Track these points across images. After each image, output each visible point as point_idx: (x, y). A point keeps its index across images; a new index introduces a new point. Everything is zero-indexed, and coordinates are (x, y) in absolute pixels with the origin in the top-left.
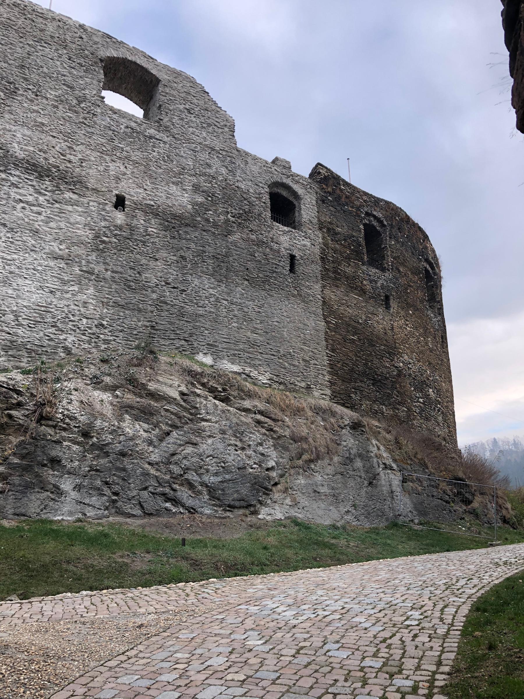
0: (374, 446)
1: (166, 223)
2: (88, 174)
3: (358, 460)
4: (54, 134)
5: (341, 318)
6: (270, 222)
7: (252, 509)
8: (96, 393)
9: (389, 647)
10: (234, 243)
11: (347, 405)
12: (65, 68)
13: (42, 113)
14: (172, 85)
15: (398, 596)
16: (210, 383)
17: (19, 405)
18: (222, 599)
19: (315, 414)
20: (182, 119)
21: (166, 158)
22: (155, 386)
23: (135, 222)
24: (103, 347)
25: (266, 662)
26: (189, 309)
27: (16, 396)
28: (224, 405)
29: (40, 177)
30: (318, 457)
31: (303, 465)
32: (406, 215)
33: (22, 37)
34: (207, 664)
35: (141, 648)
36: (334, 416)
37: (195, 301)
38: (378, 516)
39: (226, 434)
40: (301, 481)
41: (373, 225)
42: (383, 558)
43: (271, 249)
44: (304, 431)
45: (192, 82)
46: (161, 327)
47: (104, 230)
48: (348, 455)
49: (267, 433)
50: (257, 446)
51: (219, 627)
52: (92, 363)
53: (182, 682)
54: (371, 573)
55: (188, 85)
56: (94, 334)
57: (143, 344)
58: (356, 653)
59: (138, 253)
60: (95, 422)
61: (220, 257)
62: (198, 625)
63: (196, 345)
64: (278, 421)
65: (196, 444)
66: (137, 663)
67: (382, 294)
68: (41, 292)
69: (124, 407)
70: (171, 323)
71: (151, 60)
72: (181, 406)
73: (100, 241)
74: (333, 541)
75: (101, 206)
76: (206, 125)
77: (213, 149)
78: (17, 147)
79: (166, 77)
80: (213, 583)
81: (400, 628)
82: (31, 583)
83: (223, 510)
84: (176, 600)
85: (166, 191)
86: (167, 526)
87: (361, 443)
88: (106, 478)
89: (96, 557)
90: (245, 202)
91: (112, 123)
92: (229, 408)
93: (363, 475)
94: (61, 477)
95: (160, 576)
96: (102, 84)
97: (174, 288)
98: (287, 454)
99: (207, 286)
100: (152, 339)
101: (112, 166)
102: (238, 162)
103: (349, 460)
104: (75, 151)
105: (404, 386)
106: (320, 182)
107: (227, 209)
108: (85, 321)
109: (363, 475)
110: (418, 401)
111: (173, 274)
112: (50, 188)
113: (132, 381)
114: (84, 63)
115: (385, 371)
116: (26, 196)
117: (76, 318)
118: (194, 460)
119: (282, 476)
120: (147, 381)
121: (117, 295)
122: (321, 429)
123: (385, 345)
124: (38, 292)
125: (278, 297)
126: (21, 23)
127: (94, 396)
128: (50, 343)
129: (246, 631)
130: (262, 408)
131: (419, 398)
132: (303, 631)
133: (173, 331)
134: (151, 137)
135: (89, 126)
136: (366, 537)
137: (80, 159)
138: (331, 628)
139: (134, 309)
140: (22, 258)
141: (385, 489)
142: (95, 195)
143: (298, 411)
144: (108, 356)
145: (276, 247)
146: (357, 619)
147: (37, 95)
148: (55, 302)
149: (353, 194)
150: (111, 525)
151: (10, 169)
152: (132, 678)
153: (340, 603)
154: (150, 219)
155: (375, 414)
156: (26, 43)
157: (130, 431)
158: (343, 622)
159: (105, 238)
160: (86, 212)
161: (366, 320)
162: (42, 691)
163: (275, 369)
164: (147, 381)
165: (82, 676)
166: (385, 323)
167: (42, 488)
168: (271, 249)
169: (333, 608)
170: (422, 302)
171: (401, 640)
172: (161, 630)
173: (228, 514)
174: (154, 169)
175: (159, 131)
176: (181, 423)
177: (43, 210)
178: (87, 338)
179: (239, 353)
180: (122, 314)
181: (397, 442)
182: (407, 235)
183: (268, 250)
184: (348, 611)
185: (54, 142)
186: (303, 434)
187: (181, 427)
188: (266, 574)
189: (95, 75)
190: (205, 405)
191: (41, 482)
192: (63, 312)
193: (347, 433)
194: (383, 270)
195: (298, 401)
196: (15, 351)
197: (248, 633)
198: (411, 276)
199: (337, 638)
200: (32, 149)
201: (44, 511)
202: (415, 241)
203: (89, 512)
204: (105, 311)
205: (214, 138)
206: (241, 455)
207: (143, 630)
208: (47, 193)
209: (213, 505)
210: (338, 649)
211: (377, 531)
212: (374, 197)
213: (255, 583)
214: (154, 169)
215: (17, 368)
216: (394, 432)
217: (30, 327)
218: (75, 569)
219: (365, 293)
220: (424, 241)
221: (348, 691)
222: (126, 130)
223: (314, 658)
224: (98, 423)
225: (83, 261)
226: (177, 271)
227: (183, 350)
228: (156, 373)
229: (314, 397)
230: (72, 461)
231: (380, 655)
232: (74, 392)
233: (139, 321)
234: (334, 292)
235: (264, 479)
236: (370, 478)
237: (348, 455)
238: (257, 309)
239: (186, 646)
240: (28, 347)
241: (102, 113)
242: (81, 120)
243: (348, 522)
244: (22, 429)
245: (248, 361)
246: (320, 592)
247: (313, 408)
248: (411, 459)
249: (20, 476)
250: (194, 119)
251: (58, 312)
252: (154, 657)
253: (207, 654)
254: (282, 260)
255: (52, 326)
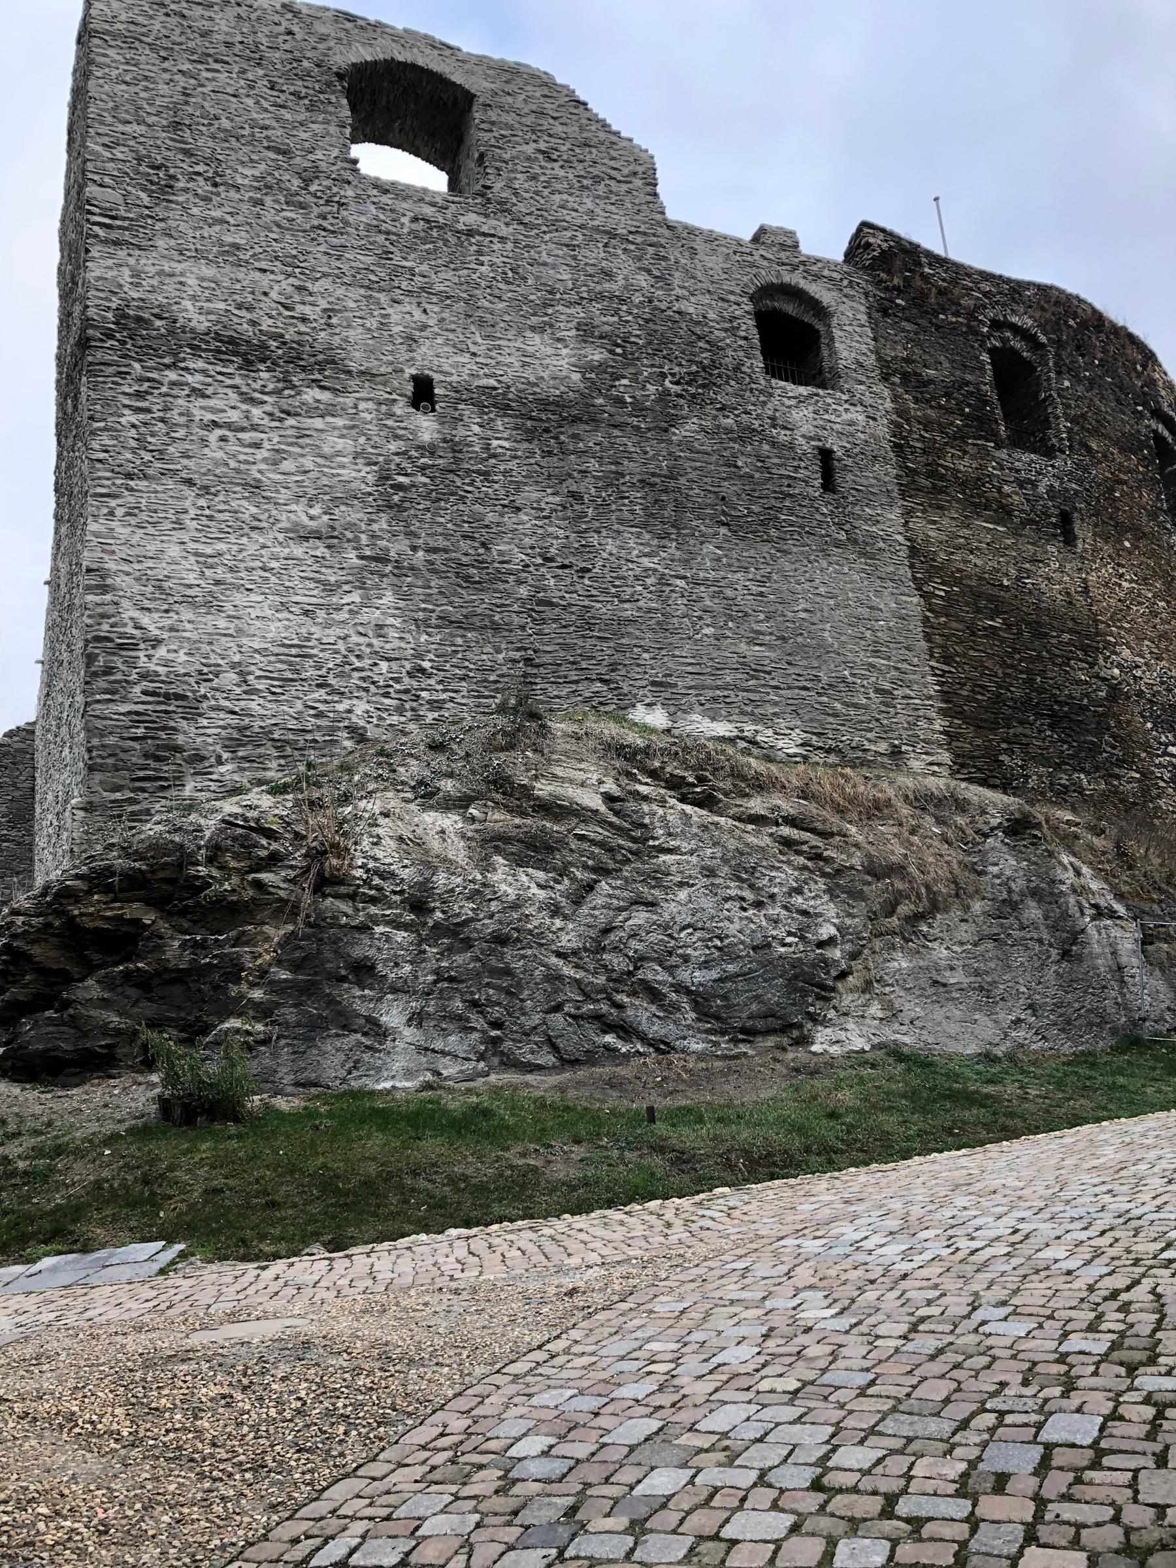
0: (1066, 869)
1: (529, 423)
2: (346, 340)
3: (1032, 903)
4: (263, 265)
5: (958, 582)
6: (763, 382)
7: (795, 1033)
8: (429, 817)
9: (1125, 1308)
10: (687, 445)
11: (991, 781)
12: (266, 110)
13: (232, 221)
14: (503, 100)
15: (1146, 1197)
16: (668, 769)
17: (274, 860)
18: (744, 1229)
19: (918, 812)
20: (534, 178)
21: (510, 274)
22: (549, 788)
23: (461, 432)
24: (430, 716)
25: (844, 1352)
26: (602, 609)
27: (264, 842)
28: (704, 812)
29: (248, 365)
30: (935, 907)
31: (901, 926)
32: (1094, 311)
33: (165, 59)
34: (715, 1361)
35: (575, 1334)
36: (964, 811)
37: (613, 590)
38: (1091, 1024)
39: (716, 876)
40: (901, 962)
41: (1012, 348)
42: (1110, 1118)
43: (773, 444)
44: (896, 851)
45: (546, 84)
46: (546, 659)
47: (397, 459)
48: (1005, 895)
49: (810, 864)
50: (790, 895)
51: (739, 1286)
52: (411, 755)
53: (666, 1399)
54: (1080, 1152)
55: (538, 94)
56: (406, 691)
57: (513, 701)
58: (1048, 1324)
59: (476, 501)
60: (434, 879)
61: (657, 480)
62: (694, 1285)
63: (626, 690)
64: (832, 835)
65: (653, 904)
66: (569, 1365)
67: (1052, 510)
68: (286, 615)
69: (490, 841)
70: (565, 647)
71: (448, 52)
72: (611, 824)
73: (392, 486)
74: (989, 1089)
75: (384, 408)
76: (590, 182)
77: (612, 235)
78: (190, 308)
79: (486, 85)
80: (724, 1196)
81: (1151, 1267)
82: (346, 1219)
83: (730, 1040)
84: (645, 1237)
85: (518, 349)
86: (613, 1083)
87: (1035, 863)
88: (472, 993)
89: (470, 1159)
90: (701, 344)
91: (382, 217)
92: (716, 819)
93: (1046, 936)
94: (380, 999)
95: (608, 1190)
96: (348, 131)
97: (564, 567)
98: (860, 908)
99: (635, 552)
100: (530, 687)
101: (395, 314)
102: (674, 254)
103: (1009, 906)
104: (311, 294)
105: (1129, 722)
106: (872, 267)
107: (661, 367)
108: (384, 666)
109: (1046, 936)
110: (1165, 754)
111: (558, 534)
112: (271, 387)
113: (500, 783)
114: (304, 91)
115: (1077, 692)
116: (224, 411)
117: (366, 663)
118: (654, 937)
119: (854, 956)
120: (531, 779)
121: (445, 601)
122: (935, 843)
123: (1070, 631)
124: (279, 615)
125: (803, 553)
126: (158, 26)
127: (425, 822)
128: (319, 722)
129: (797, 1291)
130: (792, 811)
131: (1167, 745)
132: (925, 1283)
133: (573, 663)
134: (470, 233)
135: (333, 232)
136: (1066, 1075)
137: (325, 310)
138: (990, 1276)
139: (484, 627)
140: (235, 548)
141: (1102, 964)
142: (367, 384)
143: (877, 809)
144: (442, 735)
145: (783, 436)
146: (1048, 1254)
147: (215, 185)
148: (317, 632)
149: (954, 282)
150: (496, 1091)
151: (184, 360)
152: (561, 1395)
153: (1009, 1221)
154: (492, 420)
155: (1061, 796)
156: (175, 70)
157: (509, 890)
158: (1015, 1262)
159: (401, 479)
160: (353, 427)
161: (1018, 579)
162: (382, 1429)
163: (811, 720)
164: (531, 779)
165: (460, 1394)
166: (1066, 579)
167: (344, 1027)
168: (773, 444)
169: (993, 1234)
170: (1153, 516)
171: (1153, 1292)
172: (616, 1298)
173: (743, 1048)
174: (487, 304)
175: (487, 216)
176: (616, 862)
177: (263, 436)
178: (395, 702)
179: (726, 693)
180: (459, 641)
181: (1121, 854)
182: (1101, 360)
183: (766, 447)
184: (1027, 1237)
185: (265, 283)
186: (894, 858)
187: (616, 871)
188: (840, 1170)
189: (331, 113)
190: (663, 818)
191: (340, 1014)
192: (337, 652)
193: (998, 845)
194: (1049, 452)
195: (875, 786)
196: (250, 747)
197: (802, 1295)
198: (1119, 458)
199: (1003, 1294)
200: (222, 306)
201: (355, 1073)
202: (1121, 371)
203: (445, 1068)
204: (424, 638)
205: (613, 208)
206: (755, 919)
207: (579, 1301)
208: (266, 398)
209: (708, 1032)
210: (1005, 1319)
211: (1090, 1059)
212: (1008, 281)
213: (815, 1190)
214: (487, 304)
215: (260, 782)
216: (1113, 832)
217: (274, 693)
218: (430, 1186)
219: (1009, 514)
220: (1144, 367)
221: (1031, 1404)
222: (414, 226)
223: (950, 1338)
224: (441, 879)
225: (363, 536)
226: (566, 528)
227: (601, 703)
228: (549, 760)
229: (911, 773)
230: (397, 965)
231: (1103, 1327)
232: (382, 821)
233: (499, 651)
234: (934, 522)
235: (814, 966)
236: (1064, 942)
237: (1005, 895)
238: (755, 589)
239: (670, 1327)
240: (276, 736)
241: (358, 196)
242: (316, 223)
243: (1023, 1046)
244: (286, 909)
245: (749, 709)
246: (961, 1201)
247: (911, 797)
248: (1160, 889)
249: (295, 1006)
250: (561, 173)
251: (327, 655)
252: (603, 1352)
253: (715, 1342)
254: (803, 464)
255: (319, 686)
